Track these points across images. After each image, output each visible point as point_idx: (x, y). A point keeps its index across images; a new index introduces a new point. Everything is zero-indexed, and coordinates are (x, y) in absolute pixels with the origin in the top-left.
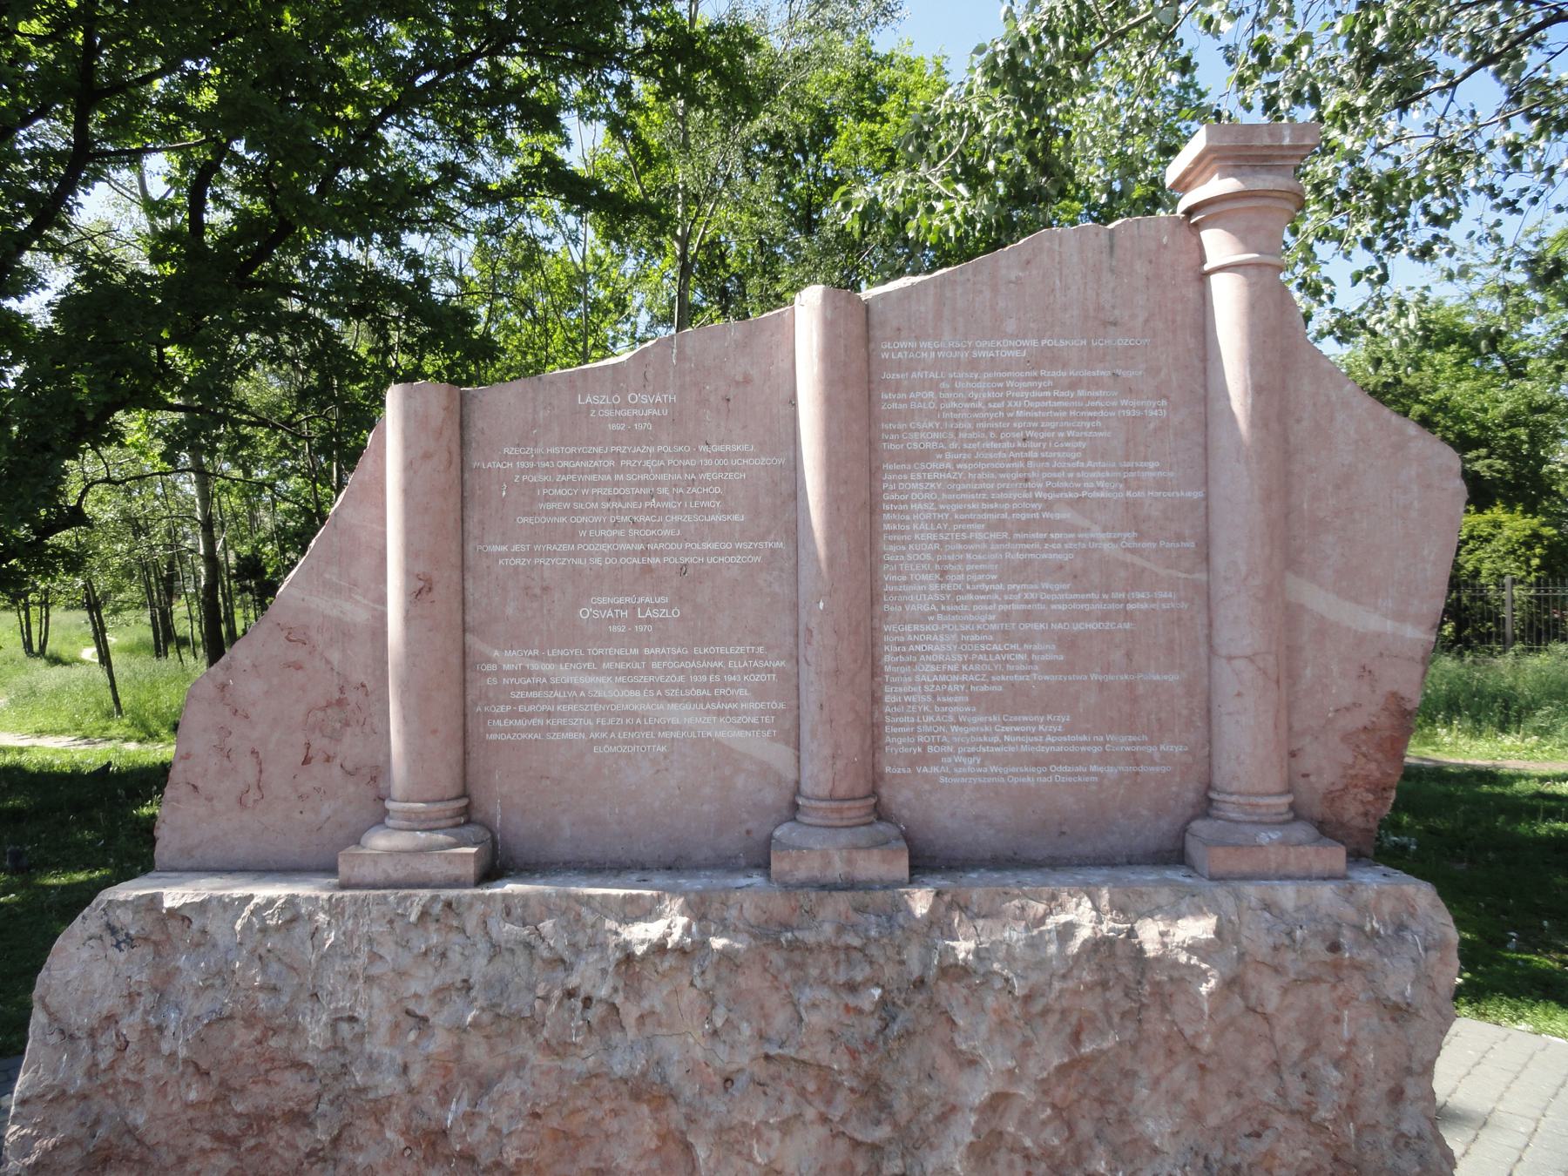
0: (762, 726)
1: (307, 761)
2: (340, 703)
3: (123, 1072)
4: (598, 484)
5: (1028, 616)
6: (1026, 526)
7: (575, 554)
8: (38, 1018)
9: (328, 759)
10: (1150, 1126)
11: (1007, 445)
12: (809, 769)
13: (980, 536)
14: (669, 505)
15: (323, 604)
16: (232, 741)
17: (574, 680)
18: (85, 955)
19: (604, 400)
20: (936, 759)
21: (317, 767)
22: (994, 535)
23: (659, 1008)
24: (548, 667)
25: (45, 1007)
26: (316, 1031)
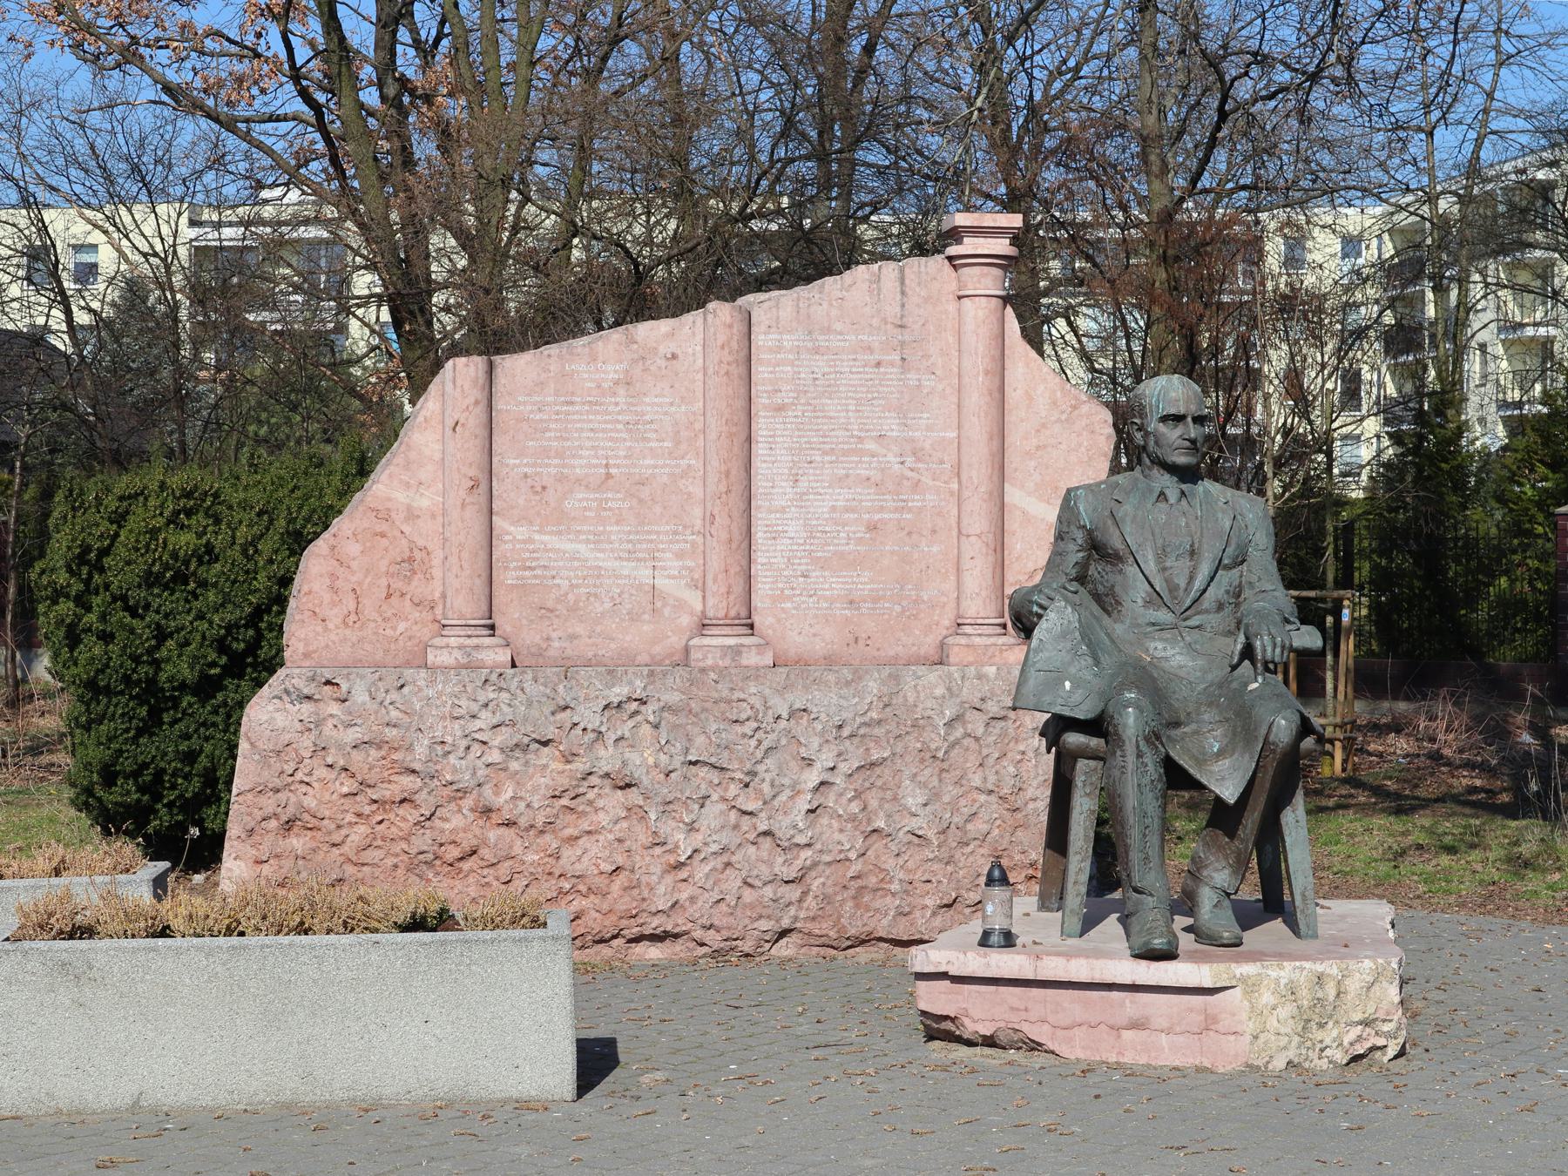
0: (681, 577)
1: (389, 596)
2: (411, 560)
3: (299, 776)
4: (580, 421)
5: (847, 510)
6: (846, 453)
7: (564, 466)
8: (243, 746)
9: (403, 595)
10: (910, 801)
11: (601, 452)
12: (711, 602)
13: (818, 459)
14: (624, 435)
15: (401, 497)
16: (339, 583)
17: (562, 547)
18: (270, 708)
19: (583, 367)
20: (789, 598)
21: (394, 600)
22: (827, 458)
23: (627, 734)
24: (546, 538)
25: (249, 739)
26: (421, 750)
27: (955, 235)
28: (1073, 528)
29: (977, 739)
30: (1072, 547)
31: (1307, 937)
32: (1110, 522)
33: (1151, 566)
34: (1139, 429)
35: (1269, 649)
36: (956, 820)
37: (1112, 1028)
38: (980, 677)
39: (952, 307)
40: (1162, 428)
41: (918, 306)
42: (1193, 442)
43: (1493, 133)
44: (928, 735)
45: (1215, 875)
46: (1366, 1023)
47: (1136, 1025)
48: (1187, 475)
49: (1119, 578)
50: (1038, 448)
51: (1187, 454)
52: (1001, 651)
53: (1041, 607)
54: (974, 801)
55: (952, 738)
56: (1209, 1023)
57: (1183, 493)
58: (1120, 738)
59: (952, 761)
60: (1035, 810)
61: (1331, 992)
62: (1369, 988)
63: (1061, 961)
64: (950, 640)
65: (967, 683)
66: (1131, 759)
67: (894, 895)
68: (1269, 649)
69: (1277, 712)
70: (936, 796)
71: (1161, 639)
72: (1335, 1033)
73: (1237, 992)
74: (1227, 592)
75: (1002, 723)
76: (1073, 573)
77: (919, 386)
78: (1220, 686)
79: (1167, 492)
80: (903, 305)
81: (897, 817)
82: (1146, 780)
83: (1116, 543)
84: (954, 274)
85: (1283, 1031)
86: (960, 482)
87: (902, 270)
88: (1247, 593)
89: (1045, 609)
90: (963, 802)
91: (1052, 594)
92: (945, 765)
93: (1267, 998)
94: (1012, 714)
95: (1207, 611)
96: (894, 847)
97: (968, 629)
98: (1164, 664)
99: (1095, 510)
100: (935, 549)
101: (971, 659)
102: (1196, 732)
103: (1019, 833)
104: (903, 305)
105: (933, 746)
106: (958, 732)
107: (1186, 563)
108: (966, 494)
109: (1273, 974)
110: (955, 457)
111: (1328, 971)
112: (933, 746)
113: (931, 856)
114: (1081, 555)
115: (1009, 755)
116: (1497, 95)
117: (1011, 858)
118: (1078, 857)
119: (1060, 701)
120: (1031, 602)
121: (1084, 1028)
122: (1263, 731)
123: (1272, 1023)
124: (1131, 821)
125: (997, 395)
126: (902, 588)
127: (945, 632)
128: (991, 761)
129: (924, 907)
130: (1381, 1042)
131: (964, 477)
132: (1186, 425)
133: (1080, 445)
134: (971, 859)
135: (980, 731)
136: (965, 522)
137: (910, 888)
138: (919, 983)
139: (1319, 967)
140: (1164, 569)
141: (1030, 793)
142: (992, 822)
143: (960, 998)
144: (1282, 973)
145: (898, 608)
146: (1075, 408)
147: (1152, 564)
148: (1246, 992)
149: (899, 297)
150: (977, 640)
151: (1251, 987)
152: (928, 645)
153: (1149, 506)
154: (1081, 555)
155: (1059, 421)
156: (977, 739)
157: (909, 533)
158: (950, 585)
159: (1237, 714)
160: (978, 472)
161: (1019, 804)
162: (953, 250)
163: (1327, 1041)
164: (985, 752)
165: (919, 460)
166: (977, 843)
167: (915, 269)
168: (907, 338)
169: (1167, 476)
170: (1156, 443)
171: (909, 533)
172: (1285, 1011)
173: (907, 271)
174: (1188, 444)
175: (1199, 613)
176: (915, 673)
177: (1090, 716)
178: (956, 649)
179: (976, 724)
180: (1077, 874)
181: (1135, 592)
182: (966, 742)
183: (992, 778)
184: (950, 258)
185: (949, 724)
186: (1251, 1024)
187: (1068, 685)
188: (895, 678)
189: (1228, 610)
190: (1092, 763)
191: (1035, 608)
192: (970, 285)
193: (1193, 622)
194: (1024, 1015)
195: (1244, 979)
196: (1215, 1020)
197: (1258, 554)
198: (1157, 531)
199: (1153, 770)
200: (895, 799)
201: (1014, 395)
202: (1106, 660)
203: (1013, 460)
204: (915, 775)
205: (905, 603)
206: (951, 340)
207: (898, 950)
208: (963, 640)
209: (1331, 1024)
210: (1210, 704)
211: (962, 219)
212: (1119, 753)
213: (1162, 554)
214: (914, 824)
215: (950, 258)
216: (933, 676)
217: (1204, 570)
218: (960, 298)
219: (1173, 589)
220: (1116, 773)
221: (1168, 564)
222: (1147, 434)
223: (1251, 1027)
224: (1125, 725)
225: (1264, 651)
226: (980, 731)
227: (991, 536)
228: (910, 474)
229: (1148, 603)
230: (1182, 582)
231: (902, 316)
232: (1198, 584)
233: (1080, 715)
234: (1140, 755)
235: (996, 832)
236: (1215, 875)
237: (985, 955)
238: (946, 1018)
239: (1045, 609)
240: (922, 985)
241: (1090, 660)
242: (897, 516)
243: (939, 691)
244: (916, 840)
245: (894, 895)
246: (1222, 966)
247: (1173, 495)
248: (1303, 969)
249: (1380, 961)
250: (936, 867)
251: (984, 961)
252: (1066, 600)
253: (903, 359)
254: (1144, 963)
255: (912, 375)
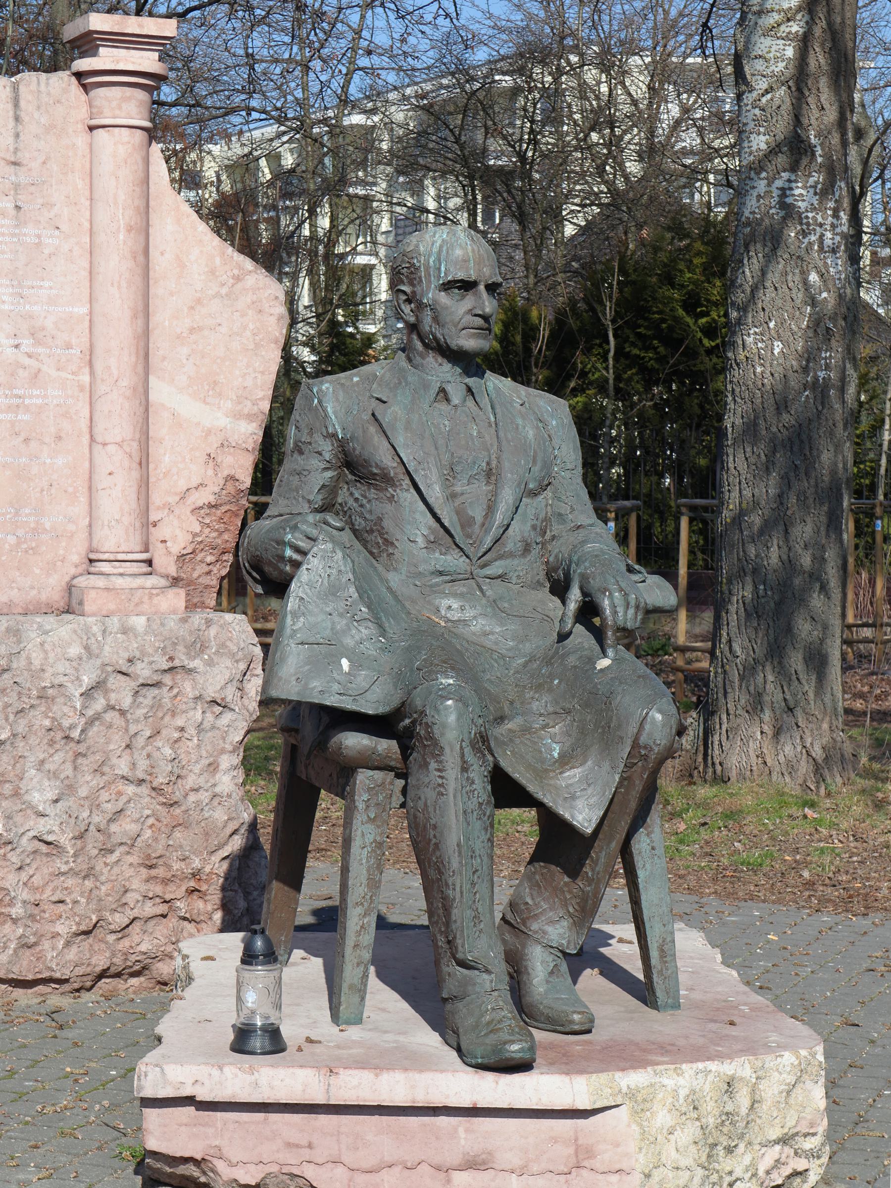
27: (87, 43)
28: (318, 438)
29: (123, 713)
30: (316, 463)
31: (666, 1006)
32: (373, 429)
33: (435, 493)
34: (409, 301)
35: (620, 610)
36: (96, 819)
37: (438, 1169)
38: (125, 630)
39: (81, 139)
40: (443, 298)
41: (36, 136)
42: (486, 318)
43: (360, 69)
44: (59, 709)
45: (549, 929)
46: (784, 1140)
47: (473, 1164)
48: (469, 363)
49: (389, 508)
50: (192, 330)
51: (477, 336)
52: (151, 595)
53: (297, 550)
54: (120, 794)
55: (90, 713)
56: (582, 1158)
57: (469, 390)
58: (436, 743)
59: (90, 742)
60: (198, 803)
61: (743, 1101)
62: (789, 1093)
63: (366, 1076)
64: (82, 582)
65: (109, 639)
66: (452, 773)
67: (15, 921)
68: (620, 610)
69: (650, 703)
70: (70, 788)
71: (455, 595)
72: (747, 1159)
73: (623, 1113)
74: (534, 527)
75: (155, 691)
76: (319, 500)
77: (39, 245)
78: (549, 662)
79: (449, 388)
80: (17, 136)
81: (18, 818)
82: (473, 804)
83: (383, 457)
84: (83, 97)
85: (683, 1163)
86: (92, 373)
87: (15, 88)
88: (556, 528)
89: (304, 553)
90: (104, 796)
91: (314, 532)
92: (82, 748)
93: (662, 1118)
94: (167, 679)
95: (511, 555)
96: (14, 858)
97: (105, 567)
98: (461, 630)
99: (348, 412)
100: (60, 461)
101: (112, 606)
102: (526, 730)
103: (177, 834)
104: (17, 136)
105: (66, 723)
106: (99, 704)
107: (482, 488)
108: (102, 388)
109: (670, 1081)
110: (85, 339)
111: (740, 1073)
112: (66, 723)
113: (64, 868)
114: (329, 474)
115: (164, 732)
116: (365, 34)
117: (169, 867)
118: (359, 910)
119: (336, 687)
120: (282, 543)
121: (397, 1170)
122: (632, 729)
123: (670, 1154)
124: (455, 864)
125: (141, 258)
126: (17, 514)
127: (73, 571)
128: (140, 741)
129: (55, 936)
130: (801, 1164)
131: (99, 366)
132: (478, 296)
133: (245, 328)
134: (116, 870)
135: (127, 701)
136: (98, 430)
137: (36, 911)
138: (147, 1111)
139: (728, 1068)
140: (453, 496)
141: (191, 781)
142: (141, 821)
143: (210, 1131)
144: (681, 1081)
145: (12, 539)
146: (238, 279)
147: (437, 488)
148: (635, 1112)
149: (11, 123)
150: (120, 582)
151: (640, 1103)
152: (51, 588)
153: (426, 406)
154: (329, 474)
155: (217, 295)
156: (123, 713)
157: (27, 440)
158: (80, 509)
159: (586, 705)
160: (117, 361)
161: (178, 796)
162: (83, 64)
163: (738, 1173)
164: (133, 729)
165: (38, 342)
166: (123, 849)
167: (33, 87)
168: (23, 179)
169: (447, 366)
170: (436, 319)
171: (27, 440)
172: (688, 1134)
173: (22, 89)
174: (479, 322)
175: (501, 557)
176: (40, 626)
177: (381, 710)
178: (93, 594)
179: (122, 692)
180: (358, 933)
181: (412, 527)
182: (109, 716)
183: (143, 764)
184: (79, 75)
185: (87, 694)
186: (641, 1158)
187: (345, 664)
188: (15, 633)
189: (536, 551)
190: (378, 775)
191: (289, 553)
192: (107, 112)
193: (496, 569)
194: (306, 1154)
195: (631, 1094)
196: (590, 1153)
197: (567, 474)
198: (441, 442)
199: (482, 788)
200: (16, 794)
201: (161, 262)
202: (391, 626)
203: (160, 344)
204: (42, 762)
205: (20, 532)
206: (80, 184)
207: (19, 993)
208: (100, 582)
209: (742, 1146)
210: (539, 688)
211: (98, 22)
212: (433, 765)
213: (450, 474)
214: (41, 826)
215: (79, 75)
216: (63, 630)
217: (507, 496)
218: (91, 128)
219: (466, 522)
220: (429, 794)
221: (458, 489)
222: (420, 306)
223: (641, 1162)
224: (444, 726)
225: (615, 613)
226: (127, 701)
227: (135, 445)
228: (27, 361)
229: (432, 544)
230: (478, 513)
231: (16, 150)
232: (499, 517)
233: (369, 707)
234: (465, 769)
235: (148, 833)
236: (549, 929)
237: (252, 1070)
238: (186, 1160)
239: (304, 553)
240: (152, 1115)
241: (373, 630)
242: (10, 416)
243: (75, 650)
244: (44, 848)
245: (15, 921)
246: (603, 1077)
247: (456, 393)
248: (708, 1072)
249: (804, 1053)
250: (70, 882)
251: (249, 1078)
252: (332, 540)
253: (18, 208)
254: (490, 1076)
255: (30, 230)
